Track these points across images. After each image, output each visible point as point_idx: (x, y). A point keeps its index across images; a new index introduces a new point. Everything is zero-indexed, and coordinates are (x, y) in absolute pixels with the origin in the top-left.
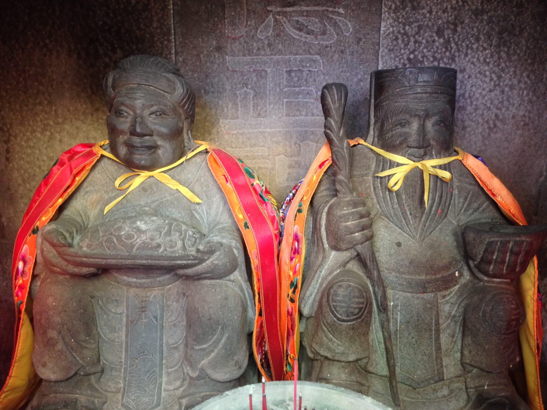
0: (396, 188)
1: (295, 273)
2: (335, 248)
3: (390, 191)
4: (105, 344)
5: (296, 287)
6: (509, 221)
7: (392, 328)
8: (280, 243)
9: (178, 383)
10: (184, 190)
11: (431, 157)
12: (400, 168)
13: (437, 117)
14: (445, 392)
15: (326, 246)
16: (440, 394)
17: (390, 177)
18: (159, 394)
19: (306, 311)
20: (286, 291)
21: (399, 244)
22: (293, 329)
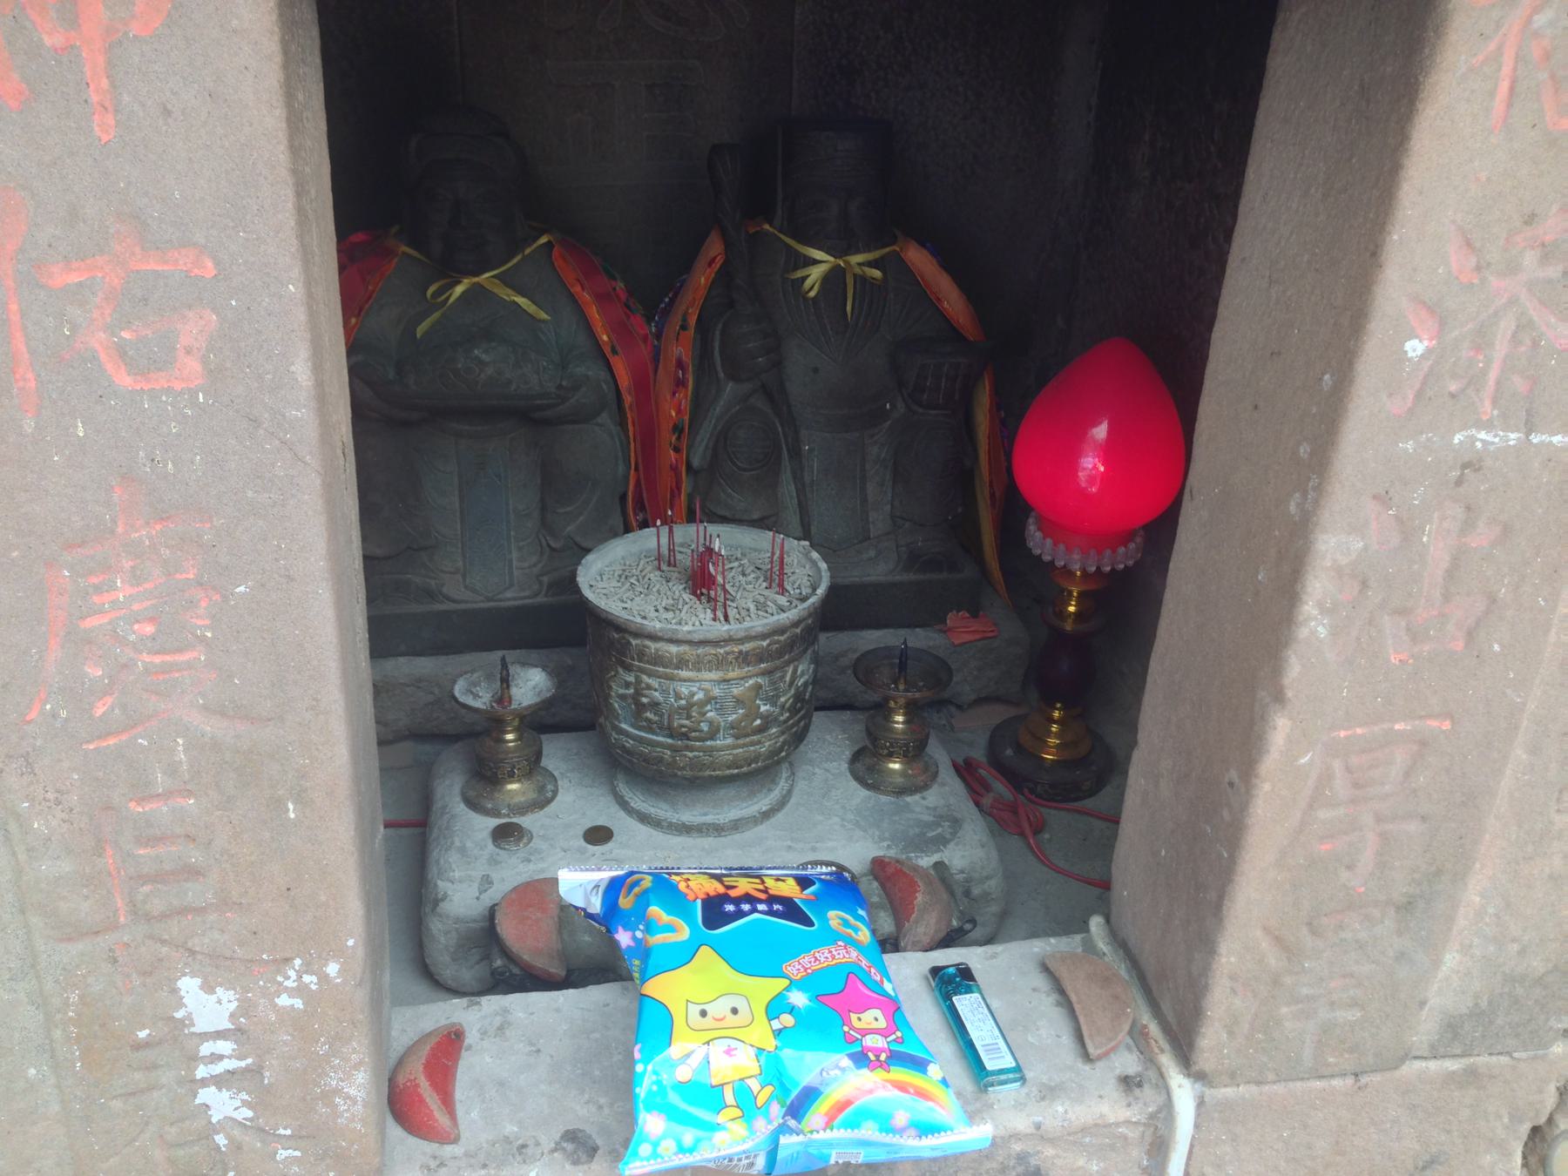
0: (812, 294)
1: (679, 411)
2: (734, 377)
3: (805, 299)
4: (1269, 145)
5: (682, 431)
6: (953, 333)
7: (807, 479)
8: (656, 371)
9: (534, 559)
10: (521, 300)
11: (858, 252)
12: (819, 265)
13: (934, 914)
14: (872, 553)
15: (722, 375)
16: (865, 556)
17: (804, 278)
18: (511, 573)
19: (696, 463)
20: (667, 437)
21: (816, 370)
22: (679, 489)
